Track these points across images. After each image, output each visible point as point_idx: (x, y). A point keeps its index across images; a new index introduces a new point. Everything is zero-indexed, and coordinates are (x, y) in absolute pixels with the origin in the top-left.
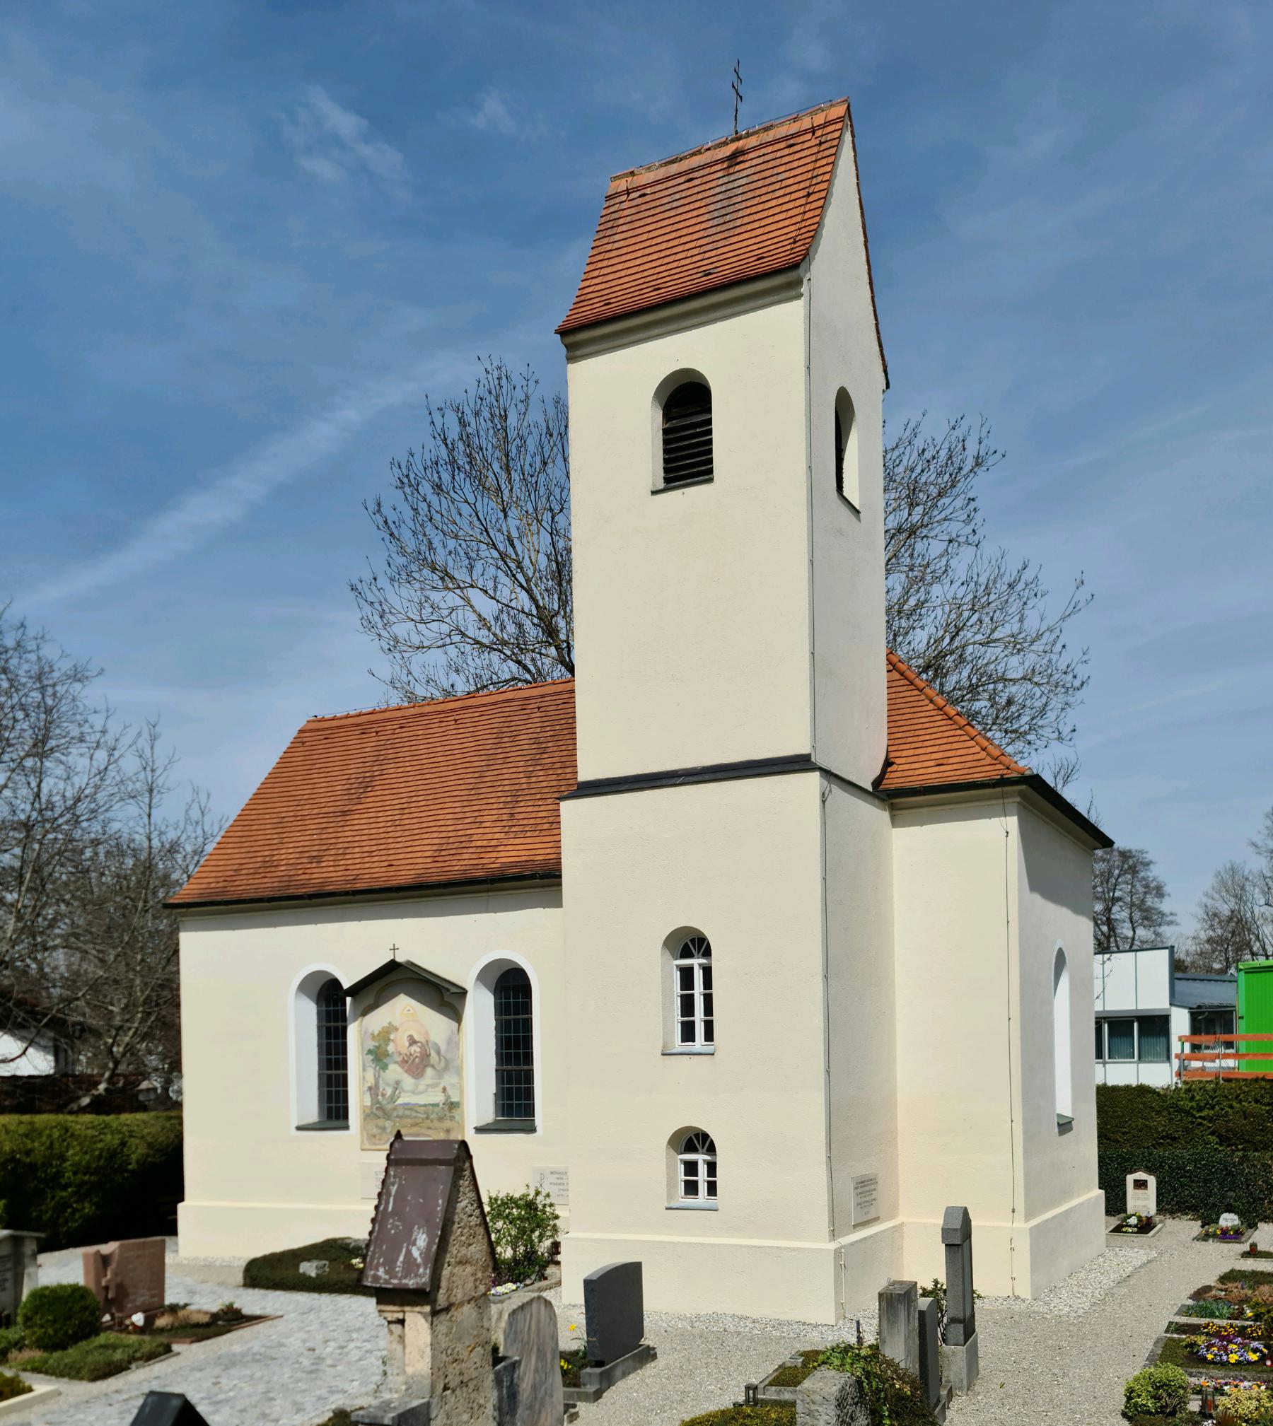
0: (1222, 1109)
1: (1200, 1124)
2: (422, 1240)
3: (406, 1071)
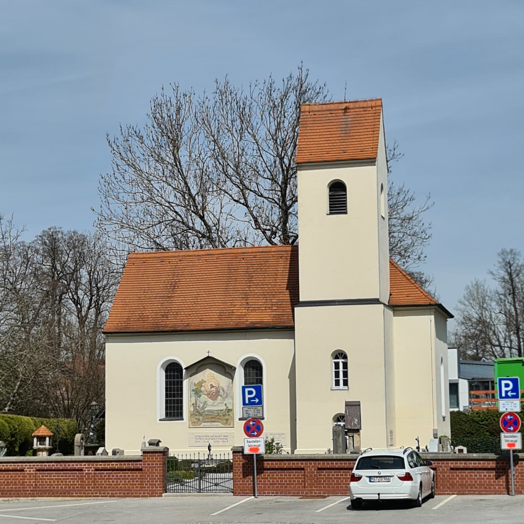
0: (491, 421)
1: (482, 427)
2: (356, 420)
3: (209, 398)
